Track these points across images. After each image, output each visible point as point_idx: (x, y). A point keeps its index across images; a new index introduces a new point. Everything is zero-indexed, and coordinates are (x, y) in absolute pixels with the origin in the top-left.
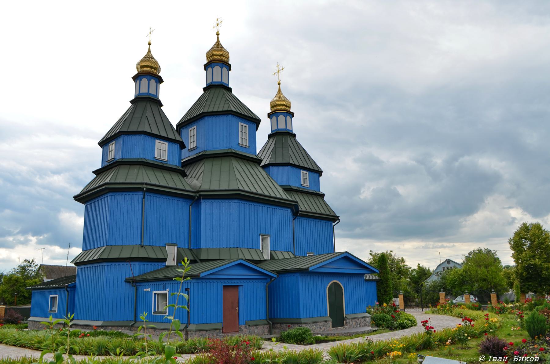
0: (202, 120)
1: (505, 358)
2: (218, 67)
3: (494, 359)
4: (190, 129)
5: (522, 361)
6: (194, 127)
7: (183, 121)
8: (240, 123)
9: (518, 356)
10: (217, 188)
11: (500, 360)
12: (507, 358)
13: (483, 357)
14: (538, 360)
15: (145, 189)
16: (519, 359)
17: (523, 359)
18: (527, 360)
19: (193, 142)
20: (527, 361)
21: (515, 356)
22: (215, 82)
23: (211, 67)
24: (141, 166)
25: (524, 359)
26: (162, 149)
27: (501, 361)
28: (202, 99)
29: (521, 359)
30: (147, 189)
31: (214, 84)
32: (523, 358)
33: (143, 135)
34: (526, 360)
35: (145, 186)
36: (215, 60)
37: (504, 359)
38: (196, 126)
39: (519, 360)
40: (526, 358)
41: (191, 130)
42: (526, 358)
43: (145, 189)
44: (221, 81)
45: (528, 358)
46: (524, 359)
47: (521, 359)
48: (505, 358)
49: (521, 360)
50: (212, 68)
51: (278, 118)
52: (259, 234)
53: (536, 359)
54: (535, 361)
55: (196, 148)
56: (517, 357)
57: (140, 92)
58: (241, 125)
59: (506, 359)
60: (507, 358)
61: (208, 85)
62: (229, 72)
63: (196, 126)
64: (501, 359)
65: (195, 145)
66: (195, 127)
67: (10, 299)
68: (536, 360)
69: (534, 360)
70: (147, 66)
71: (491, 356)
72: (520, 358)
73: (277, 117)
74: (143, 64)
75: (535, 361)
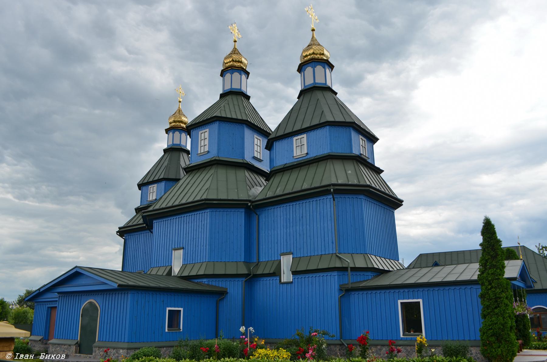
0: (213, 124)
1: (32, 356)
2: (238, 73)
3: (21, 356)
4: (200, 132)
5: (49, 358)
6: (207, 130)
7: (197, 122)
8: (255, 135)
9: (45, 354)
10: (236, 198)
11: (27, 357)
12: (33, 355)
13: (10, 355)
14: (65, 357)
15: (332, 190)
16: (45, 356)
17: (49, 356)
18: (54, 357)
19: (204, 146)
20: (54, 358)
21: (42, 354)
22: (234, 89)
23: (310, 66)
24: (329, 160)
25: (50, 357)
26: (300, 145)
27: (27, 358)
28: (217, 105)
29: (48, 357)
30: (334, 190)
31: (317, 85)
32: (50, 355)
33: (327, 127)
34: (53, 358)
35: (332, 187)
36: (235, 66)
37: (31, 356)
38: (208, 129)
39: (45, 357)
40: (52, 355)
41: (201, 133)
42: (52, 355)
43: (332, 190)
44: (240, 88)
45: (54, 355)
46: (50, 357)
47: (48, 357)
48: (32, 356)
49: (48, 357)
50: (232, 74)
51: (174, 134)
52: (279, 253)
53: (62, 356)
54: (62, 358)
55: (208, 153)
56: (43, 355)
57: (232, 87)
58: (361, 139)
59: (33, 357)
60: (33, 355)
61: (225, 92)
62: (247, 80)
63: (208, 129)
64: (28, 357)
65: (207, 149)
66: (208, 130)
67: (114, 357)
68: (63, 357)
69: (61, 357)
70: (310, 55)
71: (18, 354)
72: (47, 355)
73: (174, 133)
74: (304, 55)
75: (62, 358)
